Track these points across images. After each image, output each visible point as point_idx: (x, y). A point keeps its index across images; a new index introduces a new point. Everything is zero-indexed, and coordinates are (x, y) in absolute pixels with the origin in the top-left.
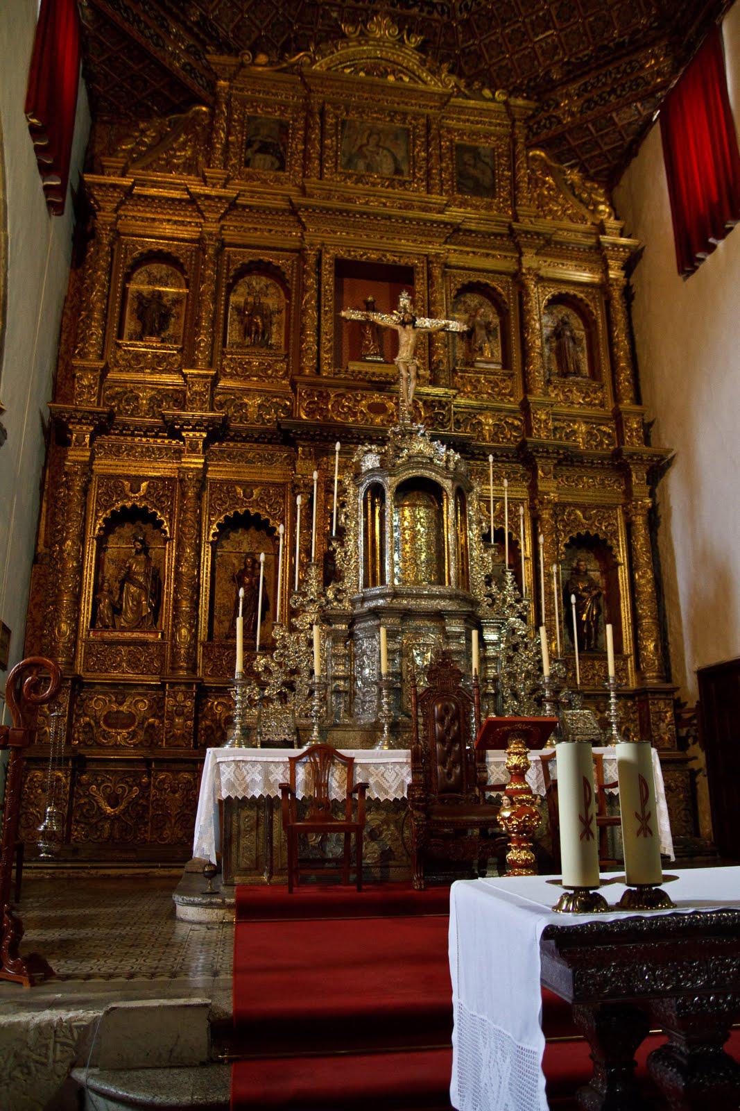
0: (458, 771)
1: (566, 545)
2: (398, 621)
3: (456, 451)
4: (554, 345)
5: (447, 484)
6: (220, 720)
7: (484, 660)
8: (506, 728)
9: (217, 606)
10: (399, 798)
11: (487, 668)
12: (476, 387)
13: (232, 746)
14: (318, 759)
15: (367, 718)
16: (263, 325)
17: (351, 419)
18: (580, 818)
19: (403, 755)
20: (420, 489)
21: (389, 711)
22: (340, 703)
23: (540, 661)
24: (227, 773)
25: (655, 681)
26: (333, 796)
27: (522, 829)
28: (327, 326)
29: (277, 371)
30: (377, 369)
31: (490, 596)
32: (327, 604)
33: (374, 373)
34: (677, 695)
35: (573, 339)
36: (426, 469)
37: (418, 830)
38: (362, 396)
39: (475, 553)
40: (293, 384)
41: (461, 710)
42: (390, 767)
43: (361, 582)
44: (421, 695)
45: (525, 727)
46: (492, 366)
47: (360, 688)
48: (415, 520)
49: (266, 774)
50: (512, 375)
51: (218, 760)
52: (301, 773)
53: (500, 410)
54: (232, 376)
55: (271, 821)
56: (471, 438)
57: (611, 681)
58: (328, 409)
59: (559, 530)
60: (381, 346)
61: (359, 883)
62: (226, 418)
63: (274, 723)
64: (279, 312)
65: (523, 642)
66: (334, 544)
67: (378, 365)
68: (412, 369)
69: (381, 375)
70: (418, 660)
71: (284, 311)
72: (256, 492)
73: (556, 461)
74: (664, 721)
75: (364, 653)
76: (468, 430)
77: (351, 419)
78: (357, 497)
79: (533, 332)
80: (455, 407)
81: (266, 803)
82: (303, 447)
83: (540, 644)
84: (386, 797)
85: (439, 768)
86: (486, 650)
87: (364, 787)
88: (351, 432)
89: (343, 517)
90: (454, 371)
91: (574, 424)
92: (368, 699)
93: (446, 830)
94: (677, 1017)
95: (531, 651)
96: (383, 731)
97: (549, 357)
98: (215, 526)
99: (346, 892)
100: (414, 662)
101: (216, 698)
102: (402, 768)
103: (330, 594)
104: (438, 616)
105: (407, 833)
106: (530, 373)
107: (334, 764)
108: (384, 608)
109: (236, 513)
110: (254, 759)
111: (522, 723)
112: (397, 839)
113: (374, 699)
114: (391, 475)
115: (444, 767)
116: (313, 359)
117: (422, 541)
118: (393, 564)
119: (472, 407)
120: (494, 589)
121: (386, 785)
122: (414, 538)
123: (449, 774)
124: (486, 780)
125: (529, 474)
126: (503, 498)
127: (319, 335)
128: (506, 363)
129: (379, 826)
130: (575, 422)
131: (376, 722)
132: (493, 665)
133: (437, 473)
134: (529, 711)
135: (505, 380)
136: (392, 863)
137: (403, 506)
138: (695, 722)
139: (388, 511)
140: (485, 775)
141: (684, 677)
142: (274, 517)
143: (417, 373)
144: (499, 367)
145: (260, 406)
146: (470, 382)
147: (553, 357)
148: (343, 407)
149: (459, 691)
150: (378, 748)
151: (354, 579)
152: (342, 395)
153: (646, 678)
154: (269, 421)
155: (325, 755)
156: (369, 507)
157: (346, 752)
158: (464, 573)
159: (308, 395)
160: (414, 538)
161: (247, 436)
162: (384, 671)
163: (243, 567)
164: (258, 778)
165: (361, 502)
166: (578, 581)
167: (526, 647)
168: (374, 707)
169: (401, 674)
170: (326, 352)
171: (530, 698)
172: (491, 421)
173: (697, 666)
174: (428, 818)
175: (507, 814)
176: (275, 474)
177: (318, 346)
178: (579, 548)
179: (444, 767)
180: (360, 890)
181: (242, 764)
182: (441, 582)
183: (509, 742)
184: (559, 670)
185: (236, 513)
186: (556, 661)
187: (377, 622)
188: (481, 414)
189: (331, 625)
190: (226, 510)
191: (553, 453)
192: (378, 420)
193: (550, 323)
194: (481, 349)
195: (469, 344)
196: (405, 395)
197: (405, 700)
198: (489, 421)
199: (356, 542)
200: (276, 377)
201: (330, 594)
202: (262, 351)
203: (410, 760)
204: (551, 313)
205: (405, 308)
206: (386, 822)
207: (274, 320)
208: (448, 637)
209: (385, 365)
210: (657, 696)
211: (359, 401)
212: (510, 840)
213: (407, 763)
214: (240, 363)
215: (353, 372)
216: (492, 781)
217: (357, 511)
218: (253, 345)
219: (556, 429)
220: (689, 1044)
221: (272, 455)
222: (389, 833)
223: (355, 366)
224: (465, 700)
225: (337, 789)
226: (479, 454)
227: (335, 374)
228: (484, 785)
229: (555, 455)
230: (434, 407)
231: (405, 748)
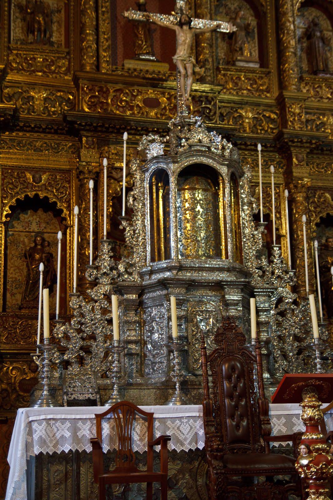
0: (245, 423)
1: (317, 225)
2: (183, 291)
3: (228, 141)
4: (305, 45)
5: (224, 170)
6: (15, 383)
8: (301, 384)
9: (9, 280)
10: (194, 449)
12: (236, 84)
13: (41, 405)
14: (121, 416)
15: (158, 378)
16: (45, 23)
17: (128, 113)
19: (195, 410)
20: (200, 175)
22: (132, 365)
24: (39, 431)
26: (135, 449)
27: (320, 476)
28: (105, 26)
29: (60, 67)
30: (149, 67)
31: (260, 268)
32: (119, 277)
33: (147, 71)
35: (323, 39)
36: (204, 156)
37: (218, 478)
38: (138, 90)
39: (247, 231)
40: (76, 80)
41: (245, 369)
42: (185, 420)
43: (149, 257)
44: (210, 356)
46: (251, 65)
47: (150, 351)
48: (194, 202)
49: (75, 430)
50: (269, 73)
51: (31, 419)
52: (106, 428)
53: (258, 105)
54: (18, 70)
55: (78, 473)
56: (235, 130)
57: (253, 343)
58: (107, 103)
59: (310, 211)
60: (152, 46)
62: (16, 110)
63: (78, 384)
64: (59, 11)
65: (290, 309)
66: (124, 223)
67: (150, 63)
68: (189, 67)
69: (154, 72)
70: (202, 326)
71: (63, 11)
72: (44, 177)
73: (308, 150)
75: (153, 320)
76: (231, 123)
77: (128, 113)
78: (143, 182)
79: (288, 33)
80: (221, 102)
81: (76, 457)
82: (87, 137)
84: (182, 448)
85: (228, 421)
87: (164, 440)
88: (130, 124)
89: (131, 200)
90: (218, 69)
91: (324, 117)
92: (158, 360)
93: (235, 478)
95: (297, 317)
97: (300, 57)
98: (7, 208)
100: (198, 327)
101: (11, 363)
102: (195, 422)
103: (121, 268)
104: (219, 286)
106: (285, 71)
108: (171, 279)
109: (27, 196)
110: (63, 416)
111: (317, 379)
112: (192, 488)
113: (163, 360)
114: (174, 162)
116: (93, 56)
117: (201, 221)
118: (177, 241)
119: (234, 102)
120: (264, 262)
121: (181, 437)
122: (194, 217)
123: (238, 426)
124: (270, 431)
125: (284, 161)
126: (271, 184)
127: (97, 34)
128: (263, 61)
129: (175, 475)
130: (324, 115)
131: (166, 381)
132: (265, 329)
133: (214, 159)
134: (297, 370)
135: (262, 78)
137: (185, 189)
139: (172, 194)
140: (268, 426)
142: (61, 200)
143: (193, 71)
144: (257, 66)
145: (45, 99)
146: (232, 79)
147: (304, 56)
148: (122, 101)
150: (171, 404)
151: (142, 253)
152: (120, 91)
154: (54, 113)
155: (127, 411)
156: (154, 191)
157: (146, 408)
158: (239, 249)
159: (90, 90)
160: (194, 217)
161: (35, 126)
162: (175, 333)
163: (33, 245)
164: (68, 434)
165: (147, 186)
166: (327, 256)
169: (187, 338)
170: (105, 51)
171: (297, 359)
172: (250, 115)
174: (225, 467)
175: (305, 462)
176: (62, 161)
177: (98, 46)
178: (327, 226)
181: (52, 422)
182: (218, 254)
183: (304, 396)
185: (27, 196)
187: (165, 292)
188: (242, 109)
189: (123, 295)
190: (17, 193)
191: (306, 143)
192: (152, 114)
193: (301, 25)
194: (241, 49)
195: (230, 44)
196: (183, 89)
198: (249, 115)
199: (143, 221)
200: (59, 73)
201: (121, 268)
202: (45, 47)
203: (202, 414)
204: (303, 16)
205: (181, 9)
206: (180, 471)
207: (55, 19)
208: (227, 304)
209: (159, 64)
211: (135, 96)
212: (308, 486)
213: (199, 417)
214: (26, 59)
215: (129, 69)
217: (143, 194)
218: (36, 42)
219: (307, 121)
221: (58, 145)
223: (130, 64)
224: (248, 359)
225: (139, 444)
226: (241, 144)
227: (113, 71)
228: (267, 436)
229: (308, 145)
230: (202, 102)
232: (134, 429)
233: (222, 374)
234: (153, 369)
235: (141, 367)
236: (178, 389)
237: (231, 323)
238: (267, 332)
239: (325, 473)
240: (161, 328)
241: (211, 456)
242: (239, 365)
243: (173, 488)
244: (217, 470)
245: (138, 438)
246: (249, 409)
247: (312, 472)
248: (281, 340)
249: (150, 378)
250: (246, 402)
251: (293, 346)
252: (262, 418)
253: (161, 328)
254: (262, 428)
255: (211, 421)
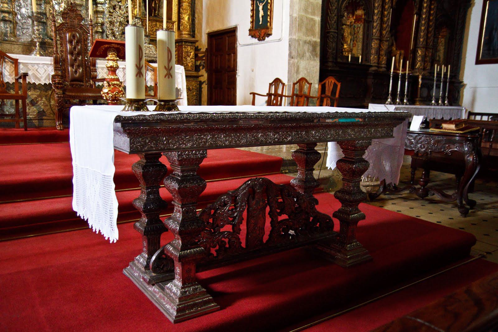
0: (81, 70)
7: (96, 12)
11: (98, 17)
15: (25, 39)
18: (136, 66)
19: (49, 60)
21: (39, 34)
22: (7, 28)
23: (128, 17)
25: (187, 36)
26: (6, 80)
34: (197, 44)
42: (41, 66)
44: (58, 27)
45: (116, 46)
47: (20, 20)
61: (26, 127)
65: (118, 5)
70: (56, 7)
74: (189, 57)
83: (127, 7)
84: (39, 82)
85: (70, 68)
86: (97, 7)
87: (25, 75)
94: (178, 160)
96: (36, 46)
99: (19, 131)
100: (54, 8)
105: (53, 102)
107: (5, 62)
112: (47, 106)
115: (73, 68)
121: (39, 76)
123: (76, 72)
129: (36, 98)
131: (31, 41)
136: (44, 117)
138: (204, 58)
140: (95, 73)
141: (201, 37)
149: (81, 27)
150: (33, 55)
153: (182, 34)
162: (34, 10)
167: (120, 8)
168: (29, 32)
173: (208, 31)
174: (64, 93)
179: (73, 68)
180: (26, 130)
183: (108, 53)
184: (138, 23)
186: (136, 18)
197: (49, 29)
203: (53, 63)
206: (40, 96)
210: (187, 44)
213: (51, 64)
216: (100, 77)
220: (182, 171)
222: (42, 102)
228: (95, 79)
231: (49, 56)
232: (5, 68)
233: (66, 39)
234: (23, 33)
235: (14, 31)
236: (38, 47)
237: (73, 7)
238: (103, 18)
239: (117, 97)
240: (27, 5)
241: (55, 87)
242: (78, 35)
243: (35, 105)
244: (58, 95)
245: (8, 74)
246: (84, 62)
247: (109, 96)
248: (111, 23)
249: (21, 38)
250: (82, 58)
251: (119, 29)
252: (92, 68)
253: (27, 5)
254: (91, 74)
255: (59, 68)
